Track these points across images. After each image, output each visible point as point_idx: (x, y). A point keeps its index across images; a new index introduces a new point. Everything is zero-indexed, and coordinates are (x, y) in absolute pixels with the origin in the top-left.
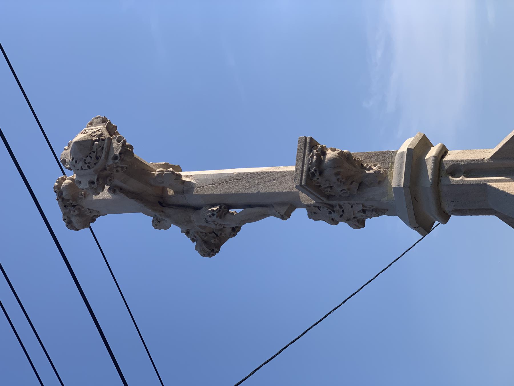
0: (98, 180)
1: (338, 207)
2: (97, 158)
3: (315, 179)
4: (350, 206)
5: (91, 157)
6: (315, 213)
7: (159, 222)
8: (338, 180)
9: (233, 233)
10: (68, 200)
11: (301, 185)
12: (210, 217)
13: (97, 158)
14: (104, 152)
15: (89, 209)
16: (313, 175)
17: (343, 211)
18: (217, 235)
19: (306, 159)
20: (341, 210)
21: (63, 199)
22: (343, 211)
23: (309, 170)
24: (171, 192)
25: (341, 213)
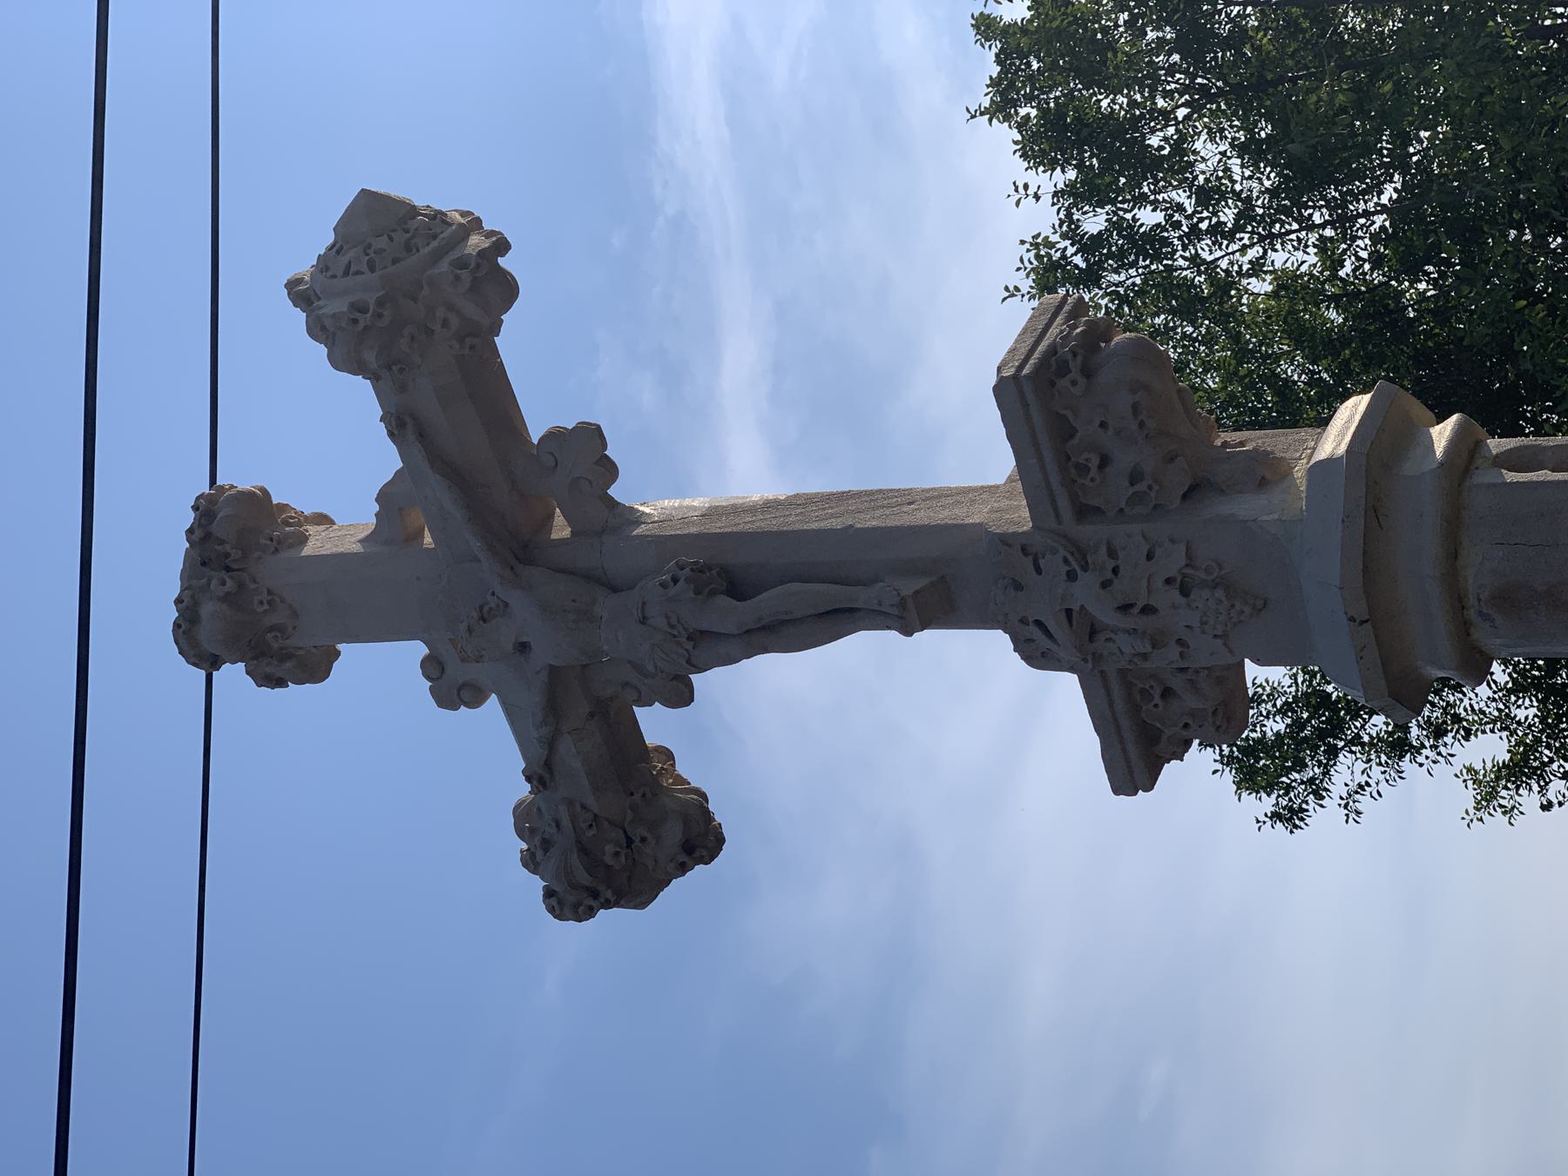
0: (380, 303)
1: (1103, 550)
2: (408, 248)
3: (1064, 383)
4: (1145, 549)
5: (391, 239)
6: (1018, 587)
7: (484, 620)
8: (1135, 408)
9: (682, 858)
10: (222, 542)
11: (1015, 377)
12: (663, 585)
13: (408, 248)
14: (435, 244)
15: (270, 592)
16: (1063, 369)
17: (1115, 571)
18: (630, 841)
19: (1053, 331)
20: (1111, 564)
21: (208, 536)
22: (1115, 571)
23: (1052, 350)
24: (561, 529)
25: (1109, 575)
